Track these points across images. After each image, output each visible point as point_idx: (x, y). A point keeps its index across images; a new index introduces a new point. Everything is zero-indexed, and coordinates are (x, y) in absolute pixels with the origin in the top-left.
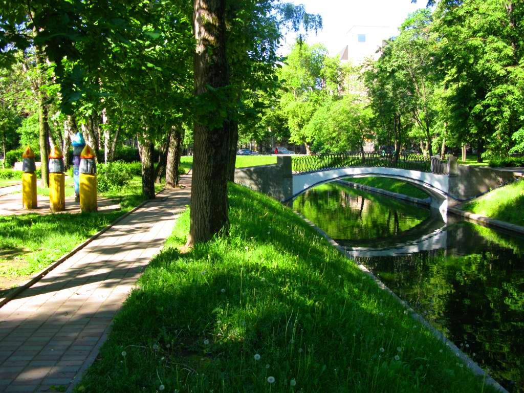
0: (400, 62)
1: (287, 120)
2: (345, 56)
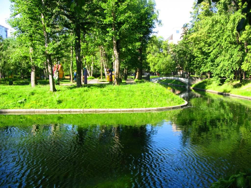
0: (180, 49)
1: (149, 63)
2: (171, 38)
